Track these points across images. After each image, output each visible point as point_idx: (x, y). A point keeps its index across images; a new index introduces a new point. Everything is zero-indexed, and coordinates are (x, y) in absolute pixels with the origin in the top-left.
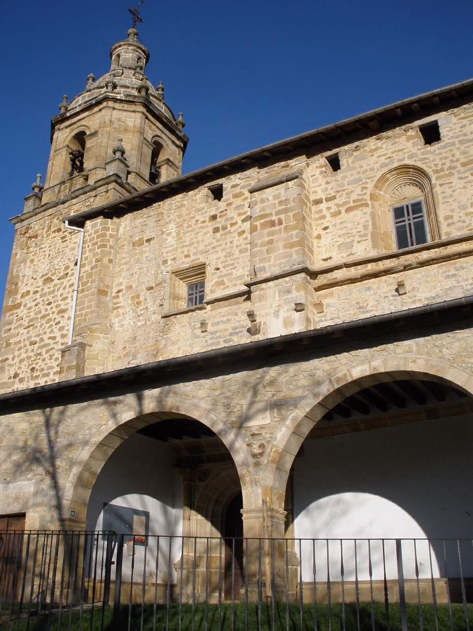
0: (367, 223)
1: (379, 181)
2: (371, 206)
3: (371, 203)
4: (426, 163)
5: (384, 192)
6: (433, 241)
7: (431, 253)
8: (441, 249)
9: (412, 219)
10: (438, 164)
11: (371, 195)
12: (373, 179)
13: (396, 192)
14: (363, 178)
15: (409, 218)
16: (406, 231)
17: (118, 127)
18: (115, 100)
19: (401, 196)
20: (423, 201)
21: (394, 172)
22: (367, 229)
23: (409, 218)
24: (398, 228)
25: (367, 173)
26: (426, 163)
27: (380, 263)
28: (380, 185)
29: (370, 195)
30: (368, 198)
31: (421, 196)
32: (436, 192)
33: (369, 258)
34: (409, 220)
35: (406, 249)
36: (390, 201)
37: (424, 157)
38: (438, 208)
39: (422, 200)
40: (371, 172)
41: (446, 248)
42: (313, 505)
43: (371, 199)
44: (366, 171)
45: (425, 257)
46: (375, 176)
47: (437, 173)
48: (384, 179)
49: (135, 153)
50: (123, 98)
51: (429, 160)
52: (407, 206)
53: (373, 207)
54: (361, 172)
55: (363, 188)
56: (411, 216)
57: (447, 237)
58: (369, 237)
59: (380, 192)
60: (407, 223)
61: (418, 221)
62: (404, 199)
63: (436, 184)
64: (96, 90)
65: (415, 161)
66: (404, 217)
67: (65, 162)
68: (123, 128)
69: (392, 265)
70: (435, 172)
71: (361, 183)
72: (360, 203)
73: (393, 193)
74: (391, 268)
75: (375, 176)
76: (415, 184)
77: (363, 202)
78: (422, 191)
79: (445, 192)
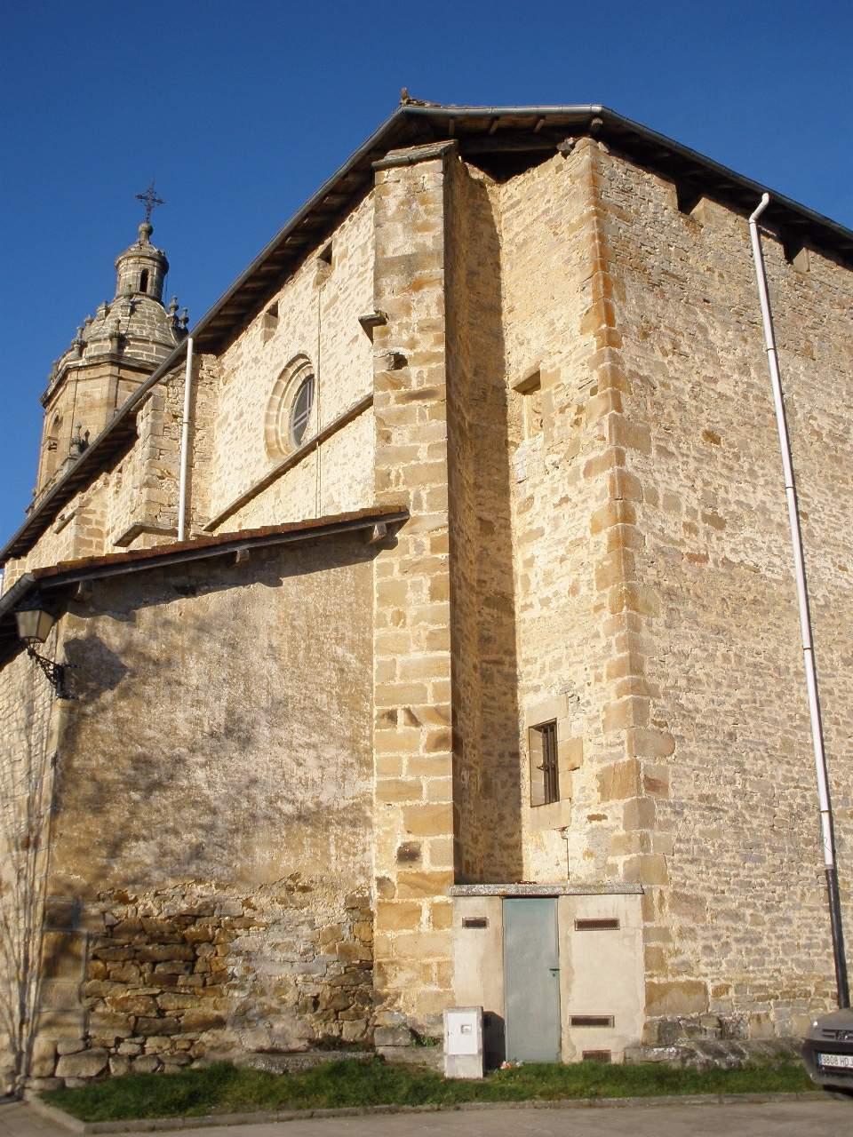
18: (79, 369)
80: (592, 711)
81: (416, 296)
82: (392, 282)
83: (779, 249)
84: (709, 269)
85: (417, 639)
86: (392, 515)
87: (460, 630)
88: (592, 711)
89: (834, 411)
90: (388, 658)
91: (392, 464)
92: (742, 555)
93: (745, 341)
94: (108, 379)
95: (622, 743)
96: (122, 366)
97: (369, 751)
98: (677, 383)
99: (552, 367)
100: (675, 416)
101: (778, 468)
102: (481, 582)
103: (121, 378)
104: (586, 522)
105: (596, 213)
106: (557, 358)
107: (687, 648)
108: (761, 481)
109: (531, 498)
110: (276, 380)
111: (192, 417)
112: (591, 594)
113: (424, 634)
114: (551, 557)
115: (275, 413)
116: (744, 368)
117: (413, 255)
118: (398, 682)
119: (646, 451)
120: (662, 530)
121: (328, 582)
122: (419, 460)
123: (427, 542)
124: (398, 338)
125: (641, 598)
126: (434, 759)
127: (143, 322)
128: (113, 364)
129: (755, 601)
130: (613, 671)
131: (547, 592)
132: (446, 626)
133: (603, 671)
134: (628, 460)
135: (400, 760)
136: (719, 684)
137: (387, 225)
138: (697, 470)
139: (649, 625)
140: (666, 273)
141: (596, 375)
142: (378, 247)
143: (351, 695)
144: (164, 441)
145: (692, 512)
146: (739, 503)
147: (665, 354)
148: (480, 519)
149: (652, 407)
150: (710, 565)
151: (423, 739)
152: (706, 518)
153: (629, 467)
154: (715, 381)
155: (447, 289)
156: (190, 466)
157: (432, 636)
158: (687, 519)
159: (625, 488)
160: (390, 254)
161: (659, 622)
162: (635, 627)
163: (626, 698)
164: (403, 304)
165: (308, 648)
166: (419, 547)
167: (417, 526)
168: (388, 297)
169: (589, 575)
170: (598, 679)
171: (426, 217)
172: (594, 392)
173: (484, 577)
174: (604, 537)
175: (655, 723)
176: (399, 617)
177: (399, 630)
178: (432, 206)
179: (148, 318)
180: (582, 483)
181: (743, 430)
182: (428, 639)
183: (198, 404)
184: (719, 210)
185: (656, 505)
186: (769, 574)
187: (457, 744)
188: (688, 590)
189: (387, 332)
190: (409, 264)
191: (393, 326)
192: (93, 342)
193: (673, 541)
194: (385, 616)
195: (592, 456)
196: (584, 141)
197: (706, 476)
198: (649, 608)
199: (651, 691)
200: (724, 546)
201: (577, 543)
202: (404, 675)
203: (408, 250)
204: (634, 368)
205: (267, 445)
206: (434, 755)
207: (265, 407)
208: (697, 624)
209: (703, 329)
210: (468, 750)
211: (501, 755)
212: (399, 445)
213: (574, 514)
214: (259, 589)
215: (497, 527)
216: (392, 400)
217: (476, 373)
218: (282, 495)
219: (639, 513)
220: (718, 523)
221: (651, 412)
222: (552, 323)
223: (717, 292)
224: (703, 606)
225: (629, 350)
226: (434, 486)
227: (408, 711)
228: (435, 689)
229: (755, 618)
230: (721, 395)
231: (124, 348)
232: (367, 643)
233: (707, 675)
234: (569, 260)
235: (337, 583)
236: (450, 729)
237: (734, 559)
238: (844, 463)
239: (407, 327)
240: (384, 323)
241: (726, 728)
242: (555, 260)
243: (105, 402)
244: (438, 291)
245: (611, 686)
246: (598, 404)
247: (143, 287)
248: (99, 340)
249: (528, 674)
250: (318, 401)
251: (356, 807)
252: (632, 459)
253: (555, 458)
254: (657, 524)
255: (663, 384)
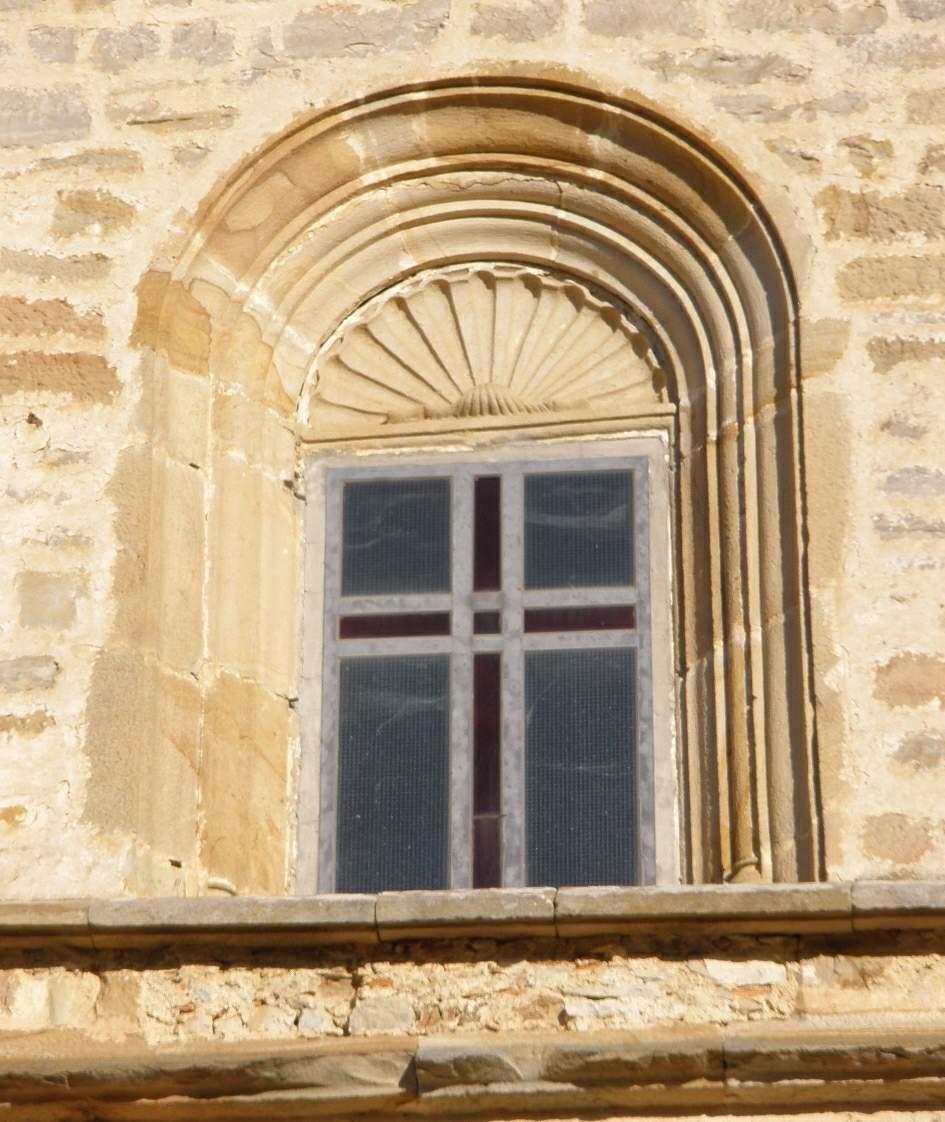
0: (66, 563)
1: (255, 170)
2: (132, 395)
3: (145, 369)
4: (766, 111)
5: (278, 298)
6: (715, 875)
7: (703, 995)
8: (809, 969)
9: (513, 620)
10: (885, 149)
11: (154, 285)
12: (200, 137)
13: (392, 328)
14: (97, 104)
15: (488, 601)
16: (440, 722)
19: (429, 371)
20: (338, 463)
21: (420, 128)
22: (66, 618)
23: (488, 601)
25: (144, 72)
26: (766, 111)
27: (152, 989)
28: (257, 210)
29: (140, 290)
30: (122, 315)
31: (642, 421)
32: (835, 403)
33: (39, 907)
34: (486, 623)
35: (397, 906)
36: (319, 400)
37: (760, 44)
38: (834, 568)
39: (643, 460)
40: (187, 70)
41: (864, 978)
43: (149, 327)
44: (139, 44)
45: (636, 1023)
46: (229, 115)
47: (861, 230)
48: (310, 172)
51: (803, 92)
52: (488, 491)
53: (154, 416)
54: (85, 47)
55: (82, 208)
56: (515, 595)
57: (887, 866)
58: (71, 702)
59: (242, 287)
60: (460, 647)
61: (582, 655)
62: (465, 410)
63: (842, 329)
65: (663, 65)
66: (440, 580)
69: (275, 1031)
70: (847, 214)
71: (64, 151)
72: (27, 343)
73: (364, 329)
74: (278, 1062)
75: (229, 115)
76: (600, 289)
77: (63, 343)
78: (663, 379)
79: (916, 433)
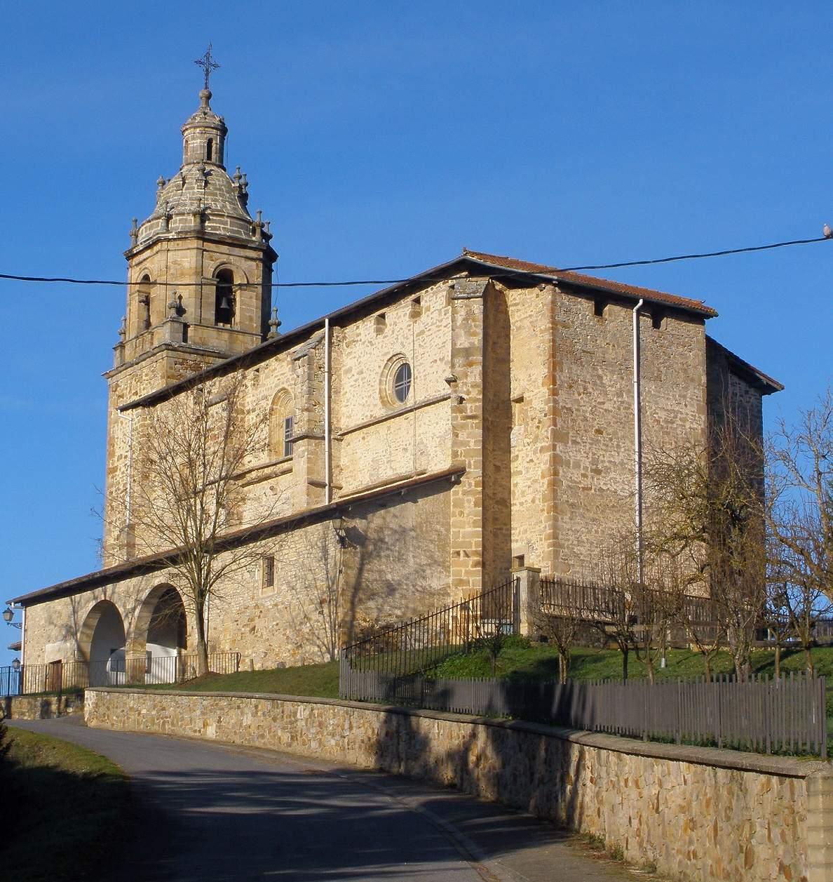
17: (175, 272)
18: (169, 240)
24: (396, 391)
42: (81, 767)
49: (193, 300)
50: (175, 237)
64: (154, 222)
67: (139, 310)
68: (179, 272)
80: (538, 552)
81: (470, 369)
82: (459, 361)
83: (649, 321)
84: (607, 344)
85: (469, 523)
86: (460, 472)
87: (485, 518)
88: (538, 552)
89: (669, 408)
90: (457, 530)
91: (459, 447)
92: (609, 486)
93: (623, 378)
94: (195, 251)
95: (548, 567)
96: (205, 240)
97: (449, 567)
98: (584, 408)
99: (529, 397)
100: (582, 424)
101: (633, 443)
102: (494, 494)
103: (205, 250)
104: (539, 473)
105: (552, 328)
106: (531, 394)
107: (578, 528)
108: (623, 450)
109: (517, 456)
110: (386, 362)
111: (330, 368)
112: (540, 504)
113: (471, 521)
114: (524, 485)
115: (385, 379)
116: (620, 394)
117: (469, 348)
118: (461, 540)
119: (566, 444)
120: (571, 478)
121: (433, 499)
122: (469, 446)
123: (473, 483)
124: (462, 390)
125: (559, 508)
126: (474, 571)
127: (216, 195)
128: (198, 238)
129: (613, 506)
130: (547, 538)
131: (523, 500)
132: (480, 518)
133: (543, 537)
134: (558, 448)
135: (461, 571)
136: (592, 543)
137: (457, 330)
138: (590, 448)
139: (562, 519)
140: (584, 351)
141: (547, 408)
142: (454, 344)
143: (442, 545)
144: (315, 383)
145: (586, 468)
146: (610, 462)
147: (580, 395)
148: (494, 465)
149: (571, 421)
150: (593, 491)
151: (471, 563)
152: (592, 470)
153: (558, 452)
154: (604, 403)
155: (484, 367)
156: (330, 397)
157: (475, 522)
158: (583, 472)
159: (556, 461)
160: (458, 346)
161: (566, 518)
162: (555, 519)
163: (551, 549)
164: (464, 373)
165: (427, 526)
166: (470, 485)
167: (468, 476)
168: (458, 369)
169: (539, 496)
170: (541, 540)
171: (475, 329)
172: (545, 415)
173: (495, 492)
174: (546, 481)
175: (562, 559)
176: (461, 513)
177: (461, 518)
178: (477, 323)
179: (220, 190)
180: (538, 455)
181: (616, 426)
182: (473, 523)
183: (332, 359)
184: (617, 308)
185: (569, 467)
186: (622, 494)
187: (484, 565)
188: (581, 503)
189: (457, 386)
190: (467, 352)
191: (460, 383)
192: (177, 215)
193: (575, 482)
194: (455, 513)
195: (543, 444)
196: (549, 287)
197: (594, 451)
198: (563, 512)
199: (562, 546)
200: (601, 482)
201: (536, 481)
202: (463, 537)
203: (467, 345)
204: (564, 404)
205: (381, 397)
206: (474, 569)
207: (379, 375)
208: (584, 518)
209: (600, 378)
210: (487, 567)
211: (501, 569)
212: (462, 439)
213: (535, 468)
214: (410, 504)
215: (502, 469)
216: (459, 419)
217: (495, 395)
218: (392, 430)
219: (561, 471)
220: (598, 472)
221: (570, 424)
222: (530, 376)
223: (610, 355)
224: (587, 510)
225: (562, 396)
226: (476, 458)
227: (464, 551)
228: (475, 543)
229: (612, 514)
230: (606, 410)
231: (205, 222)
232: (448, 524)
233: (587, 539)
234: (539, 347)
235: (437, 499)
236: (481, 559)
237: (605, 488)
238: (671, 434)
239: (465, 384)
240: (455, 381)
241: (594, 562)
242: (534, 344)
243: (194, 271)
244: (480, 368)
245: (546, 544)
246: (547, 421)
247: (209, 157)
248: (183, 214)
249: (515, 535)
250: (414, 386)
251: (444, 589)
252: (560, 447)
253: (529, 441)
254: (570, 475)
255: (577, 410)
